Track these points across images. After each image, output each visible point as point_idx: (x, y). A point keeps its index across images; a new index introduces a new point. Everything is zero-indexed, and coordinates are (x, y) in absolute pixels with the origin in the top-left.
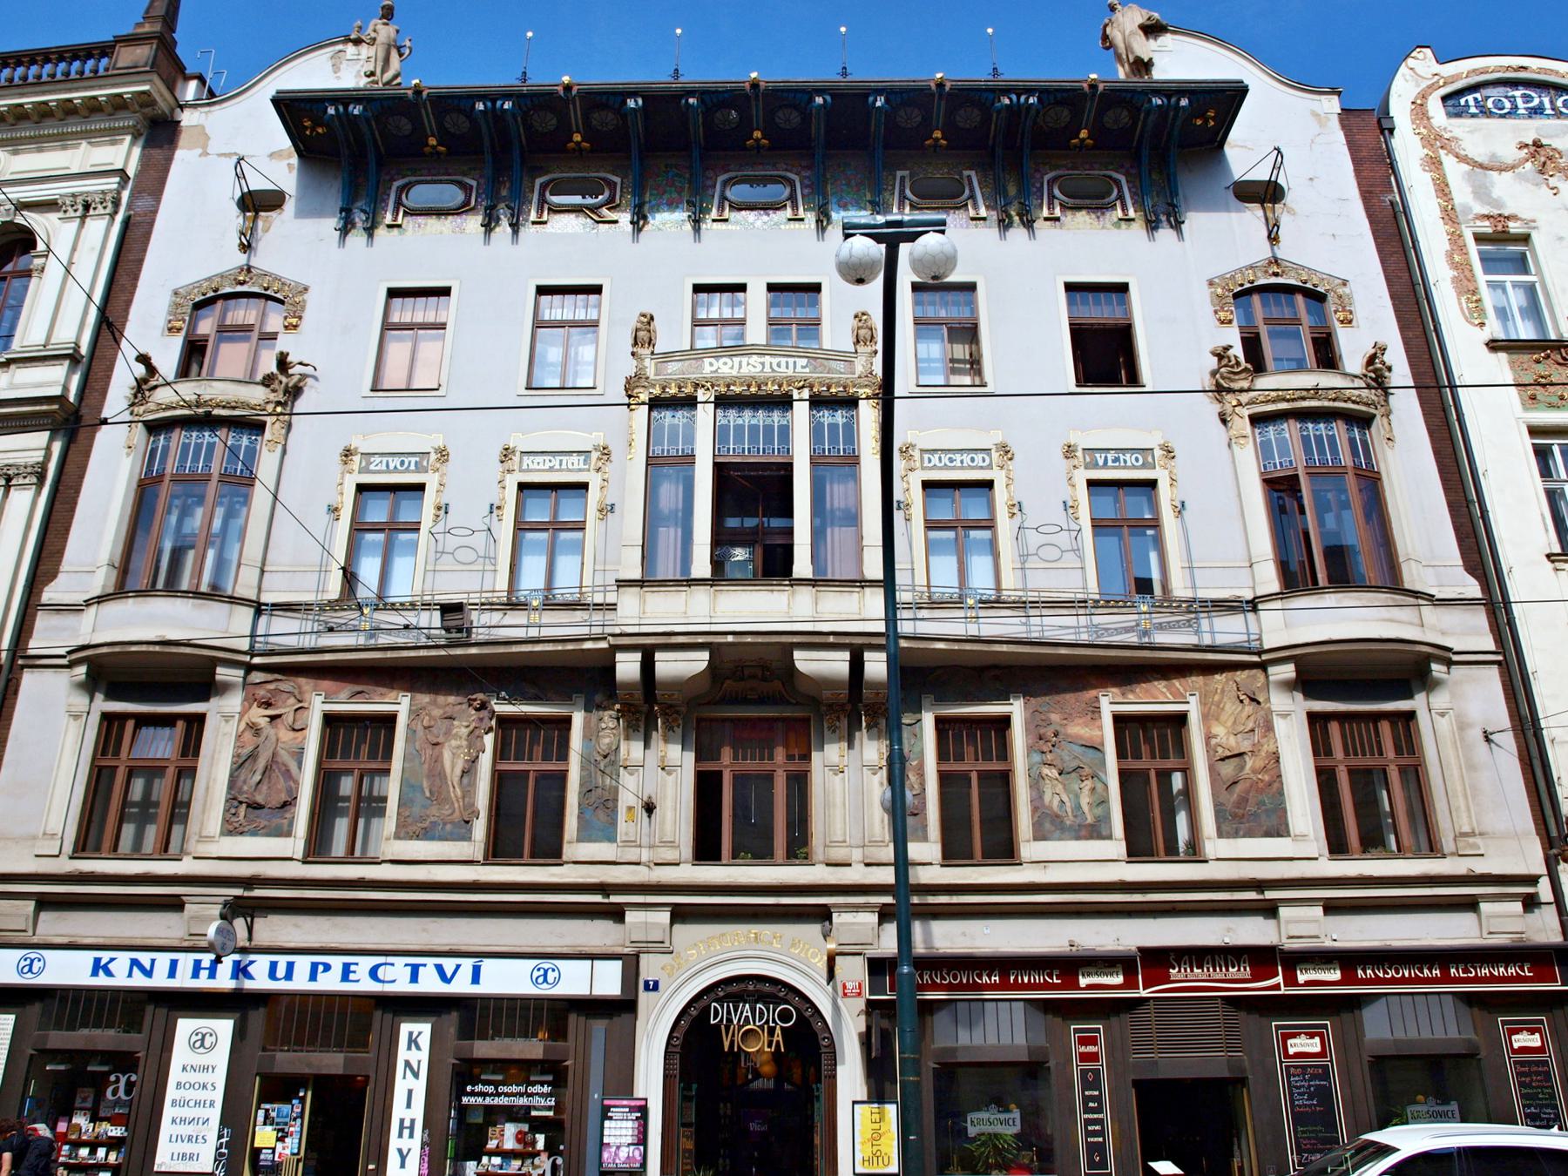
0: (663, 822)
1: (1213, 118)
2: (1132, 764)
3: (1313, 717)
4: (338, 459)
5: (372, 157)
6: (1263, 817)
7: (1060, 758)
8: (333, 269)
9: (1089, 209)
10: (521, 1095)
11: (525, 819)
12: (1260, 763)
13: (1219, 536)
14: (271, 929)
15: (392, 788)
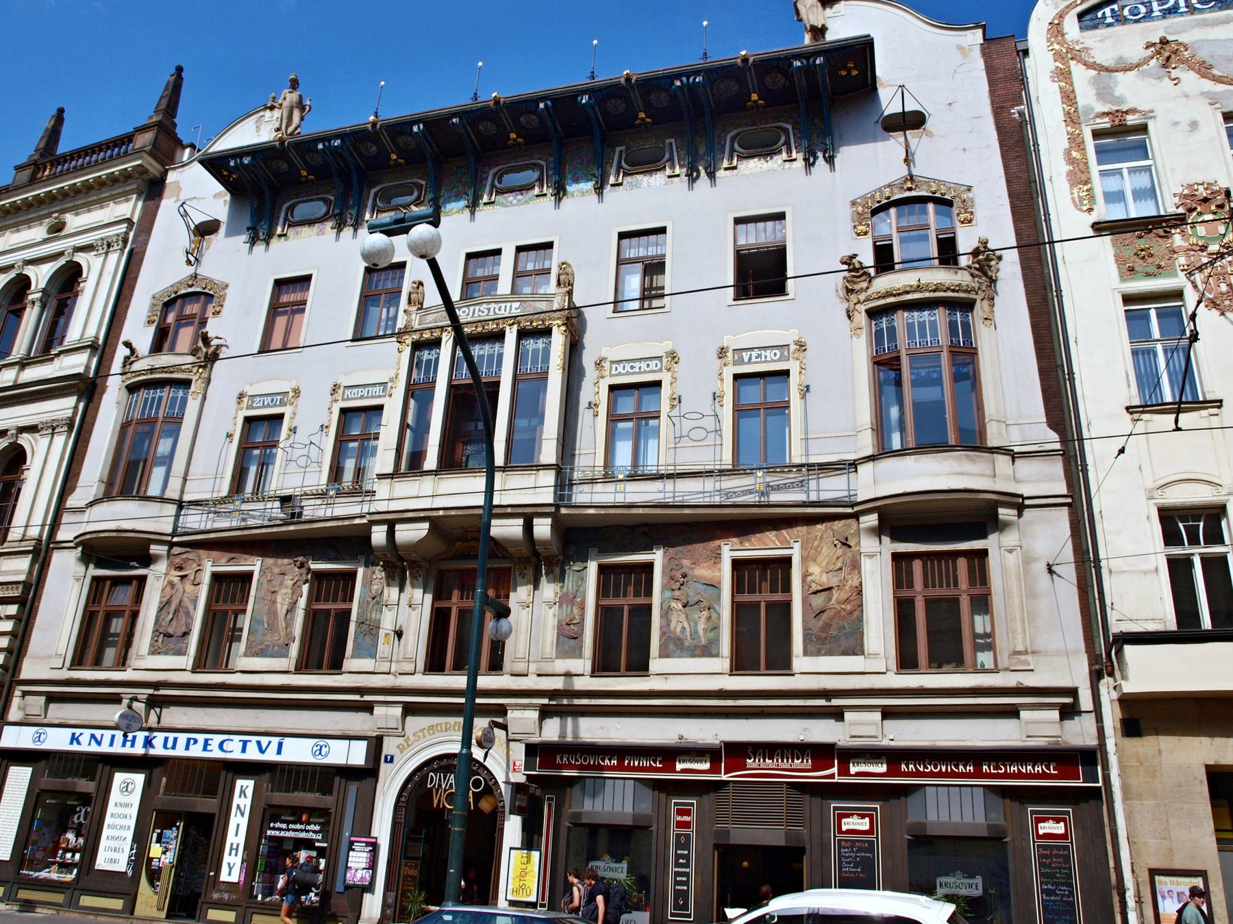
0: (406, 644)
1: (845, 68)
2: (746, 598)
3: (896, 557)
4: (235, 400)
5: (355, 177)
6: (843, 638)
7: (693, 594)
8: (243, 271)
9: (759, 156)
10: (302, 831)
11: (325, 643)
12: (844, 596)
13: (835, 409)
14: (174, 716)
15: (245, 622)
